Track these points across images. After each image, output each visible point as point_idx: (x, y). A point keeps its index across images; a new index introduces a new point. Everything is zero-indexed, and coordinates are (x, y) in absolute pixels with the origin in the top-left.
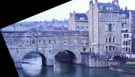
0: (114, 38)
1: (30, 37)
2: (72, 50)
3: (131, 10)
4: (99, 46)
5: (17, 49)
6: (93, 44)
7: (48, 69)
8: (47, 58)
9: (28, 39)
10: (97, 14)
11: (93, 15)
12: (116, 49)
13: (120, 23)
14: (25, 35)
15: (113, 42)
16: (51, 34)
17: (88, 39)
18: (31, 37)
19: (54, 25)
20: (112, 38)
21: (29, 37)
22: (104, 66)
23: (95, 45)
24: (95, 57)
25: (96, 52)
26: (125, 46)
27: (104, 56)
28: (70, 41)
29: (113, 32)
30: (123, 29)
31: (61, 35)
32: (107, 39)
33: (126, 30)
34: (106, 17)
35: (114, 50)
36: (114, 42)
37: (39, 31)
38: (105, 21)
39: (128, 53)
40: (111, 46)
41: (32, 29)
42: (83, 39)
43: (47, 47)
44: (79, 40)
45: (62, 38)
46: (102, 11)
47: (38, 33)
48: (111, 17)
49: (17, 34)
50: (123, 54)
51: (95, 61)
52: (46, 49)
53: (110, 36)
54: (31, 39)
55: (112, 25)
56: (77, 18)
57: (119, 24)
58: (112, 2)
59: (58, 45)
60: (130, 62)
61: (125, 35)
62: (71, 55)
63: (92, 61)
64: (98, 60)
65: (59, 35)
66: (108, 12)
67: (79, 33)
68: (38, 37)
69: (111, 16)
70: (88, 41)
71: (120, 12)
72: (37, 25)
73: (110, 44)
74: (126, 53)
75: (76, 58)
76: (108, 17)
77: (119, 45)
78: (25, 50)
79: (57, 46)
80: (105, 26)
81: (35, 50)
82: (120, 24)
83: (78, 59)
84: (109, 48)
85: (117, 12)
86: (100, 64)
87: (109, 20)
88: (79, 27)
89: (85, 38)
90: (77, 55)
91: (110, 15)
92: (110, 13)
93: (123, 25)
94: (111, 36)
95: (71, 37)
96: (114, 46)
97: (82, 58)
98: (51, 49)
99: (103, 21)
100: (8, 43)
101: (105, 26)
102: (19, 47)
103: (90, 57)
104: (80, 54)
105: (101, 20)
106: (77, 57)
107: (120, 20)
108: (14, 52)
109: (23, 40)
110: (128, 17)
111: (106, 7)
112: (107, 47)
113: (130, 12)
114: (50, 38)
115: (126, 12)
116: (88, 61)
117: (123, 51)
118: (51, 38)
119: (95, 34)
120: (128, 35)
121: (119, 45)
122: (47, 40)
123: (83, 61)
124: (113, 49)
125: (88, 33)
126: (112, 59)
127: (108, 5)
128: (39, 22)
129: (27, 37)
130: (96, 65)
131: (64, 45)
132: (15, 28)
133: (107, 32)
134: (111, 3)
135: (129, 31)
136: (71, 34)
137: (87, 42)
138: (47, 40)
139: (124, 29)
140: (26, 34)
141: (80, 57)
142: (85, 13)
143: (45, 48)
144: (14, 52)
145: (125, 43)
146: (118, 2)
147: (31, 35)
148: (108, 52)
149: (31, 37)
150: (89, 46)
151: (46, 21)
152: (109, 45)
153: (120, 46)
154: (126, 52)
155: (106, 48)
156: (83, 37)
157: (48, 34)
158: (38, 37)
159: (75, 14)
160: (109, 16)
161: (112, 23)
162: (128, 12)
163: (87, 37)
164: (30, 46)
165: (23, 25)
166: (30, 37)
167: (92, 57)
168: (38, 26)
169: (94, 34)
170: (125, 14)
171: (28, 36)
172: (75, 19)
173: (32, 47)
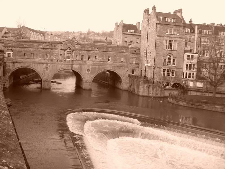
0: (174, 59)
1: (64, 50)
2: (117, 71)
3: (197, 24)
4: (154, 68)
5: (47, 64)
8: (83, 79)
9: (62, 52)
10: (155, 26)
12: (176, 74)
13: (184, 40)
14: (59, 47)
16: (92, 48)
17: (139, 59)
19: (89, 37)
20: (172, 58)
21: (63, 50)
22: (159, 95)
23: (149, 67)
24: (147, 81)
25: (149, 75)
27: (160, 82)
29: (174, 51)
31: (105, 51)
32: (166, 59)
33: (190, 50)
34: (166, 31)
35: (174, 75)
36: (173, 64)
37: (76, 43)
38: (164, 36)
39: (192, 81)
40: (170, 70)
44: (127, 59)
45: (105, 54)
47: (75, 45)
48: (172, 31)
49: (49, 45)
51: (148, 88)
52: (83, 67)
53: (170, 56)
54: (66, 52)
55: (173, 41)
56: (125, 30)
58: (173, 12)
60: (194, 93)
61: (188, 56)
62: (115, 77)
63: (143, 87)
64: (152, 87)
65: (102, 50)
66: (169, 24)
67: (128, 50)
68: (75, 51)
70: (139, 61)
71: (185, 25)
74: (189, 80)
75: (121, 82)
76: (168, 31)
77: (181, 69)
78: (57, 66)
80: (164, 43)
82: (184, 41)
84: (167, 72)
85: (180, 25)
87: (169, 36)
88: (126, 41)
89: (135, 56)
90: (124, 78)
92: (171, 26)
93: (186, 43)
95: (116, 54)
96: (174, 70)
98: (91, 68)
99: (162, 36)
100: (37, 56)
101: (164, 43)
103: (141, 82)
105: (159, 35)
106: (122, 80)
107: (184, 36)
110: (194, 32)
111: (167, 18)
113: (196, 27)
114: (90, 53)
115: (191, 26)
116: (138, 88)
117: (185, 78)
118: (91, 53)
119: (149, 53)
120: (192, 56)
121: (181, 69)
122: (86, 55)
123: (131, 86)
125: (140, 50)
126: (170, 87)
127: (168, 15)
128: (71, 32)
129: (61, 49)
130: (148, 94)
133: (166, 51)
134: (172, 13)
135: (194, 51)
138: (86, 55)
139: (188, 48)
141: (127, 80)
142: (135, 24)
143: (82, 66)
144: (42, 68)
146: (182, 13)
147: (65, 47)
149: (66, 50)
151: (80, 31)
152: (167, 68)
153: (181, 70)
154: (188, 79)
155: (163, 72)
157: (87, 48)
158: (75, 50)
160: (170, 30)
161: (173, 39)
162: (193, 26)
163: (138, 55)
164: (63, 61)
166: (64, 50)
167: (144, 83)
169: (148, 52)
170: (190, 29)
171: (63, 48)
172: (122, 31)
173: (66, 63)
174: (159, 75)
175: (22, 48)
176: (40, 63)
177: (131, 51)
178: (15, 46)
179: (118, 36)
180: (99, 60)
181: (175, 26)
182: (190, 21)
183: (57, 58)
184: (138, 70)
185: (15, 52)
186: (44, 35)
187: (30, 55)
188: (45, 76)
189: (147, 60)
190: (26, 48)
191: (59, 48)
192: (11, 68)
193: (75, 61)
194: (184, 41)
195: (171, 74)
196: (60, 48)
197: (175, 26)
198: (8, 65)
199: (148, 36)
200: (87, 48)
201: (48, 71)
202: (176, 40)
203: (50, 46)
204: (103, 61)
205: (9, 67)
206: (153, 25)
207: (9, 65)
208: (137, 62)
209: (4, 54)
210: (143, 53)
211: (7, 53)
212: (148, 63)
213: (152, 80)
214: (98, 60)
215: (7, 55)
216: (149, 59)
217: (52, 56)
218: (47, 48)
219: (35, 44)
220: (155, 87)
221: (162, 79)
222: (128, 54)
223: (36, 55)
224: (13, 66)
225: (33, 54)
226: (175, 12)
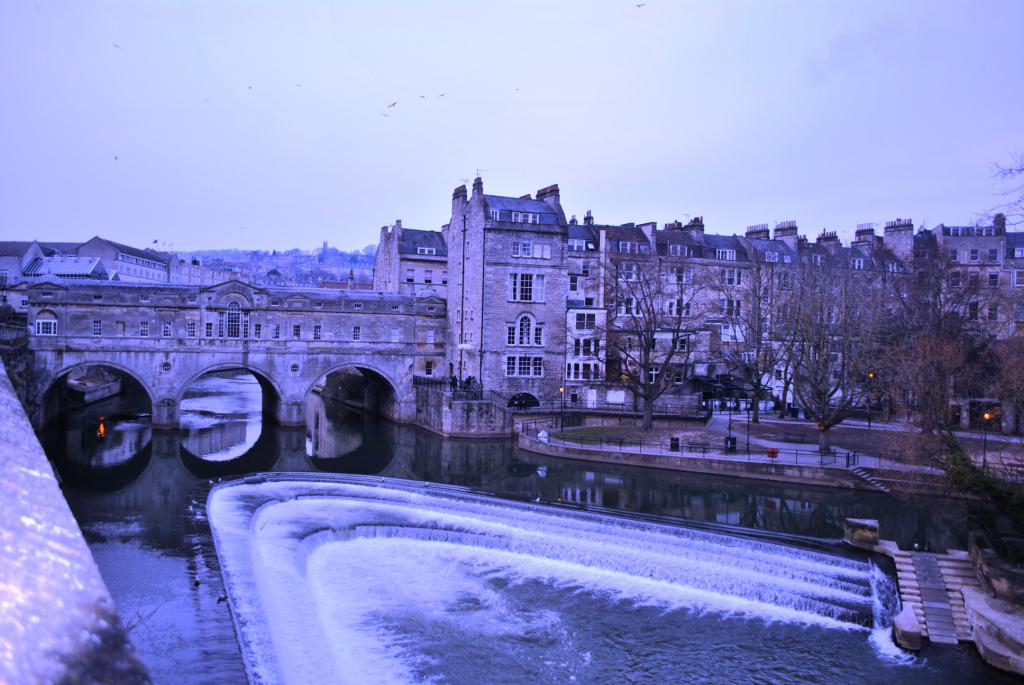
0: (539, 326)
1: (220, 311)
2: (383, 369)
4: (482, 357)
5: (167, 354)
9: (213, 318)
10: (480, 236)
11: (467, 241)
13: (565, 272)
16: (304, 304)
17: (444, 330)
18: (226, 309)
20: (533, 326)
22: (497, 431)
23: (470, 353)
26: (581, 359)
27: (499, 395)
28: (375, 333)
30: (573, 295)
31: (343, 310)
32: (514, 329)
35: (540, 374)
36: (537, 340)
37: (255, 288)
38: (506, 264)
44: (411, 330)
45: (343, 319)
46: (495, 225)
49: (172, 296)
50: (574, 387)
52: (278, 359)
53: (526, 318)
55: (534, 277)
57: (560, 275)
61: (580, 317)
64: (476, 408)
65: (334, 308)
68: (252, 314)
69: (529, 245)
73: (524, 350)
82: (564, 276)
83: (402, 404)
84: (520, 364)
87: (521, 261)
89: (431, 324)
90: (401, 387)
91: (526, 242)
92: (526, 235)
93: (574, 280)
94: (529, 320)
96: (540, 359)
97: (417, 401)
102: (176, 347)
104: (411, 384)
105: (491, 260)
107: (564, 262)
108: (154, 366)
109: (194, 318)
112: (511, 360)
113: (603, 233)
114: (298, 319)
116: (439, 413)
123: (419, 411)
124: (535, 369)
128: (266, 254)
129: (209, 309)
131: (352, 349)
133: (514, 305)
134: (534, 197)
137: (440, 339)
142: (438, 229)
145: (241, 328)
146: (557, 196)
147: (223, 302)
148: (514, 378)
149: (226, 309)
150: (447, 355)
151: (296, 251)
152: (521, 352)
154: (582, 382)
155: (509, 364)
156: (425, 318)
157: (290, 304)
164: (218, 343)
165: (201, 264)
169: (465, 309)
171: (213, 305)
172: (400, 252)
174: (497, 375)
175: (88, 305)
177: (421, 308)
178: (64, 301)
180: (327, 338)
182: (586, 219)
183: (197, 333)
184: (442, 362)
185: (64, 317)
186: (168, 264)
187: (110, 326)
188: (160, 389)
190: (100, 305)
191: (204, 307)
192: (50, 367)
196: (207, 305)
197: (537, 233)
198: (43, 358)
201: (171, 374)
204: (337, 339)
205: (46, 363)
207: (45, 359)
208: (438, 341)
209: (30, 327)
211: (38, 321)
212: (466, 341)
214: (322, 339)
215: (39, 328)
218: (167, 305)
219: (128, 296)
221: (506, 385)
222: (412, 318)
223: (133, 326)
224: (58, 362)
225: (123, 323)
226: (542, 194)
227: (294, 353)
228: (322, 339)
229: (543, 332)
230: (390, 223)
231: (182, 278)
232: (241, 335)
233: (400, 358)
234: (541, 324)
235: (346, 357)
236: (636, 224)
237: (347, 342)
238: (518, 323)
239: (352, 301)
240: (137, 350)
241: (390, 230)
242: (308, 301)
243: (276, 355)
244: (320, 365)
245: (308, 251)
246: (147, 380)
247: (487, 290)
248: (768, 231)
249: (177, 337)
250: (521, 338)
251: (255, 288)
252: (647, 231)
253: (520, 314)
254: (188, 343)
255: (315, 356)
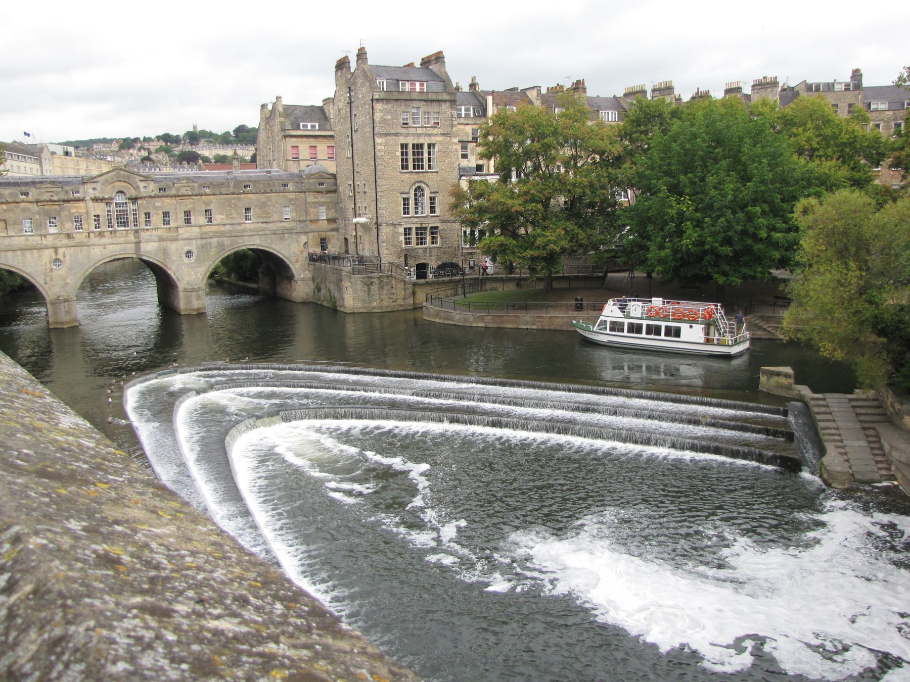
0: (433, 195)
1: (108, 201)
4: (377, 229)
5: (56, 249)
6: (355, 220)
7: (185, 327)
8: (177, 282)
9: (100, 209)
11: (353, 113)
13: (456, 140)
14: (89, 191)
15: (431, 212)
16: (193, 188)
17: (336, 205)
21: (102, 200)
22: (400, 302)
23: (364, 225)
25: (367, 250)
30: (464, 163)
32: (408, 199)
37: (141, 176)
38: (397, 135)
41: (113, 171)
42: (319, 202)
43: (177, 240)
46: (383, 95)
49: (54, 190)
50: (471, 254)
53: (419, 187)
54: (113, 208)
55: (426, 147)
59: (222, 228)
65: (223, 191)
66: (407, 99)
68: (139, 202)
69: (418, 114)
72: (131, 151)
79: (217, 232)
81: (129, 251)
82: (455, 144)
83: (300, 282)
84: (417, 234)
85: (440, 98)
86: (387, 297)
87: (411, 131)
89: (322, 200)
90: (297, 266)
91: (415, 111)
92: (415, 104)
93: (464, 148)
94: (422, 190)
95: (268, 197)
96: (436, 228)
102: (65, 241)
104: (307, 261)
107: (454, 129)
109: (80, 211)
112: (407, 231)
113: (490, 99)
114: (188, 204)
115: (477, 98)
116: (340, 289)
122: (176, 209)
124: (432, 238)
128: (136, 140)
129: (96, 200)
131: (244, 231)
132: (41, 164)
133: (408, 175)
136: (269, 185)
138: (176, 209)
140: (91, 191)
142: (321, 104)
145: (131, 218)
149: (112, 199)
155: (405, 234)
157: (178, 189)
158: (141, 198)
159: (281, 109)
161: (426, 141)
163: (332, 195)
164: (107, 234)
165: (73, 154)
166: (108, 201)
168: (133, 158)
169: (357, 183)
171: (100, 196)
172: (283, 130)
176: (30, 249)
179: (273, 142)
181: (426, 101)
189: (358, 206)
193: (143, 230)
194: (455, 144)
195: (429, 239)
196: (93, 196)
197: (426, 101)
199: (354, 138)
200: (178, 189)
201: (60, 271)
202: (433, 142)
203: (57, 193)
206: (364, 103)
208: (330, 217)
210: (345, 189)
212: (360, 215)
213: (376, 262)
216: (362, 202)
217: (70, 224)
220: (385, 280)
222: (302, 195)
226: (426, 62)
227: (186, 239)
228: (214, 222)
229: (437, 201)
230: (270, 100)
231: (54, 169)
232: (131, 225)
233: (294, 236)
234: (435, 193)
235: (240, 240)
236: (520, 89)
237: (239, 224)
238: (412, 193)
239: (241, 182)
240: (24, 247)
241: (270, 107)
242: (196, 185)
243: (169, 243)
244: (213, 250)
245: (178, 136)
246: (38, 279)
247: (378, 161)
248: (644, 92)
249: (64, 231)
250: (416, 208)
251: (141, 176)
252: (532, 95)
253: (414, 184)
254: (77, 236)
255: (208, 240)
